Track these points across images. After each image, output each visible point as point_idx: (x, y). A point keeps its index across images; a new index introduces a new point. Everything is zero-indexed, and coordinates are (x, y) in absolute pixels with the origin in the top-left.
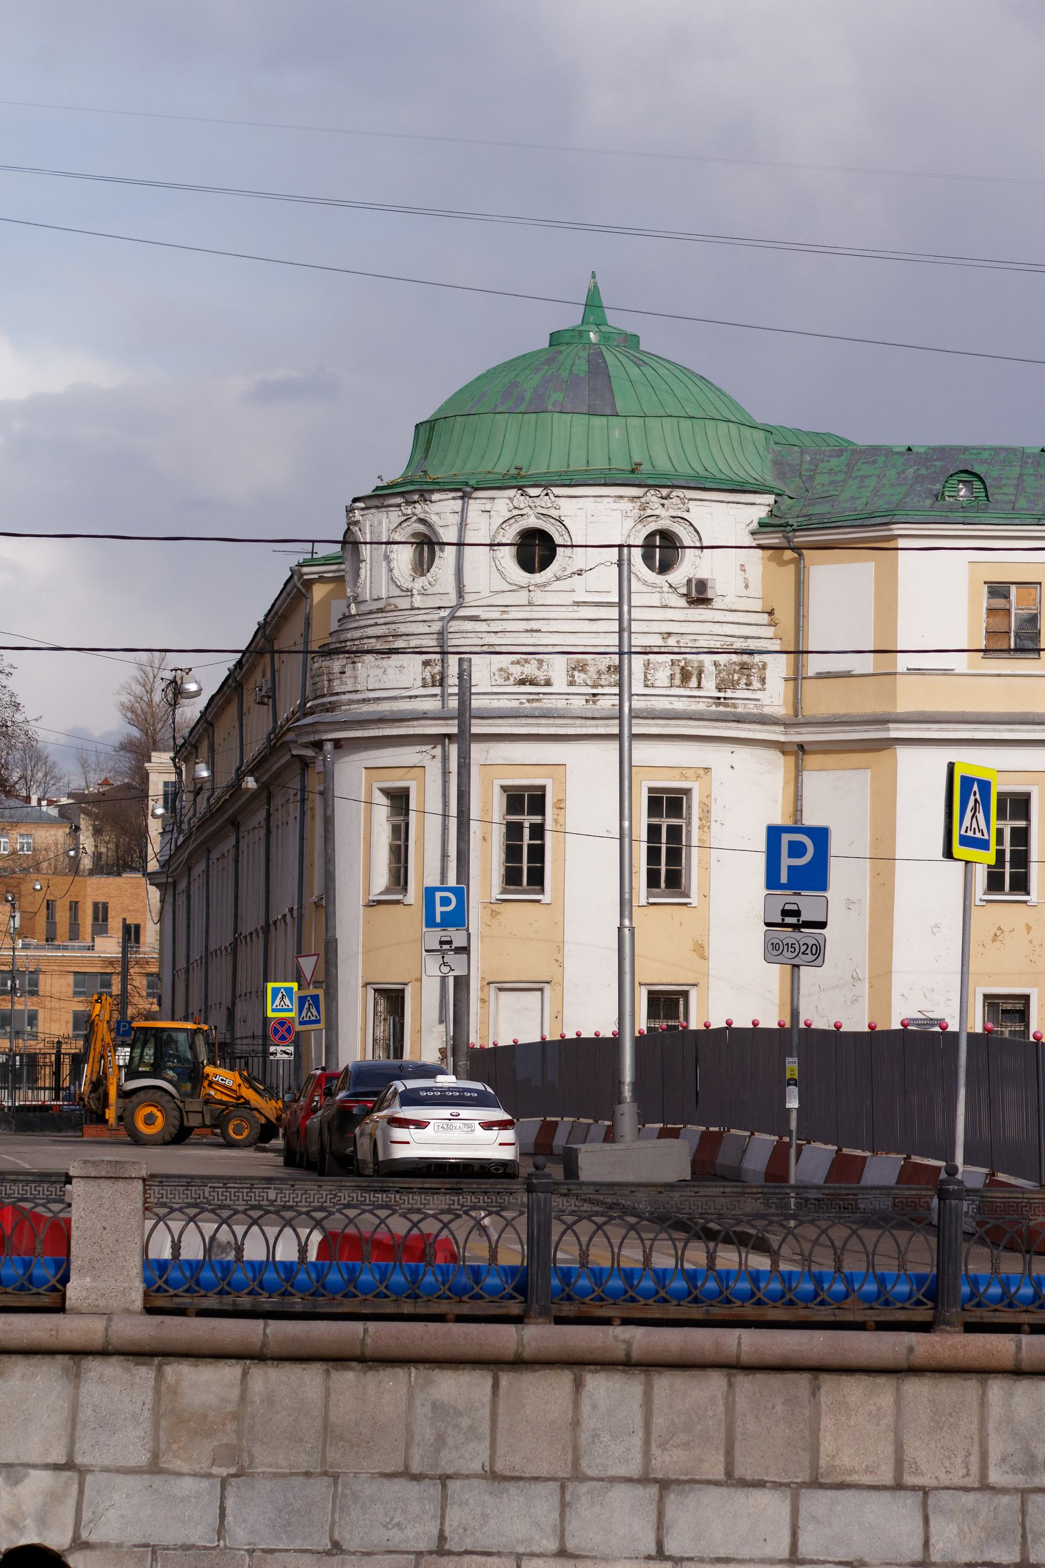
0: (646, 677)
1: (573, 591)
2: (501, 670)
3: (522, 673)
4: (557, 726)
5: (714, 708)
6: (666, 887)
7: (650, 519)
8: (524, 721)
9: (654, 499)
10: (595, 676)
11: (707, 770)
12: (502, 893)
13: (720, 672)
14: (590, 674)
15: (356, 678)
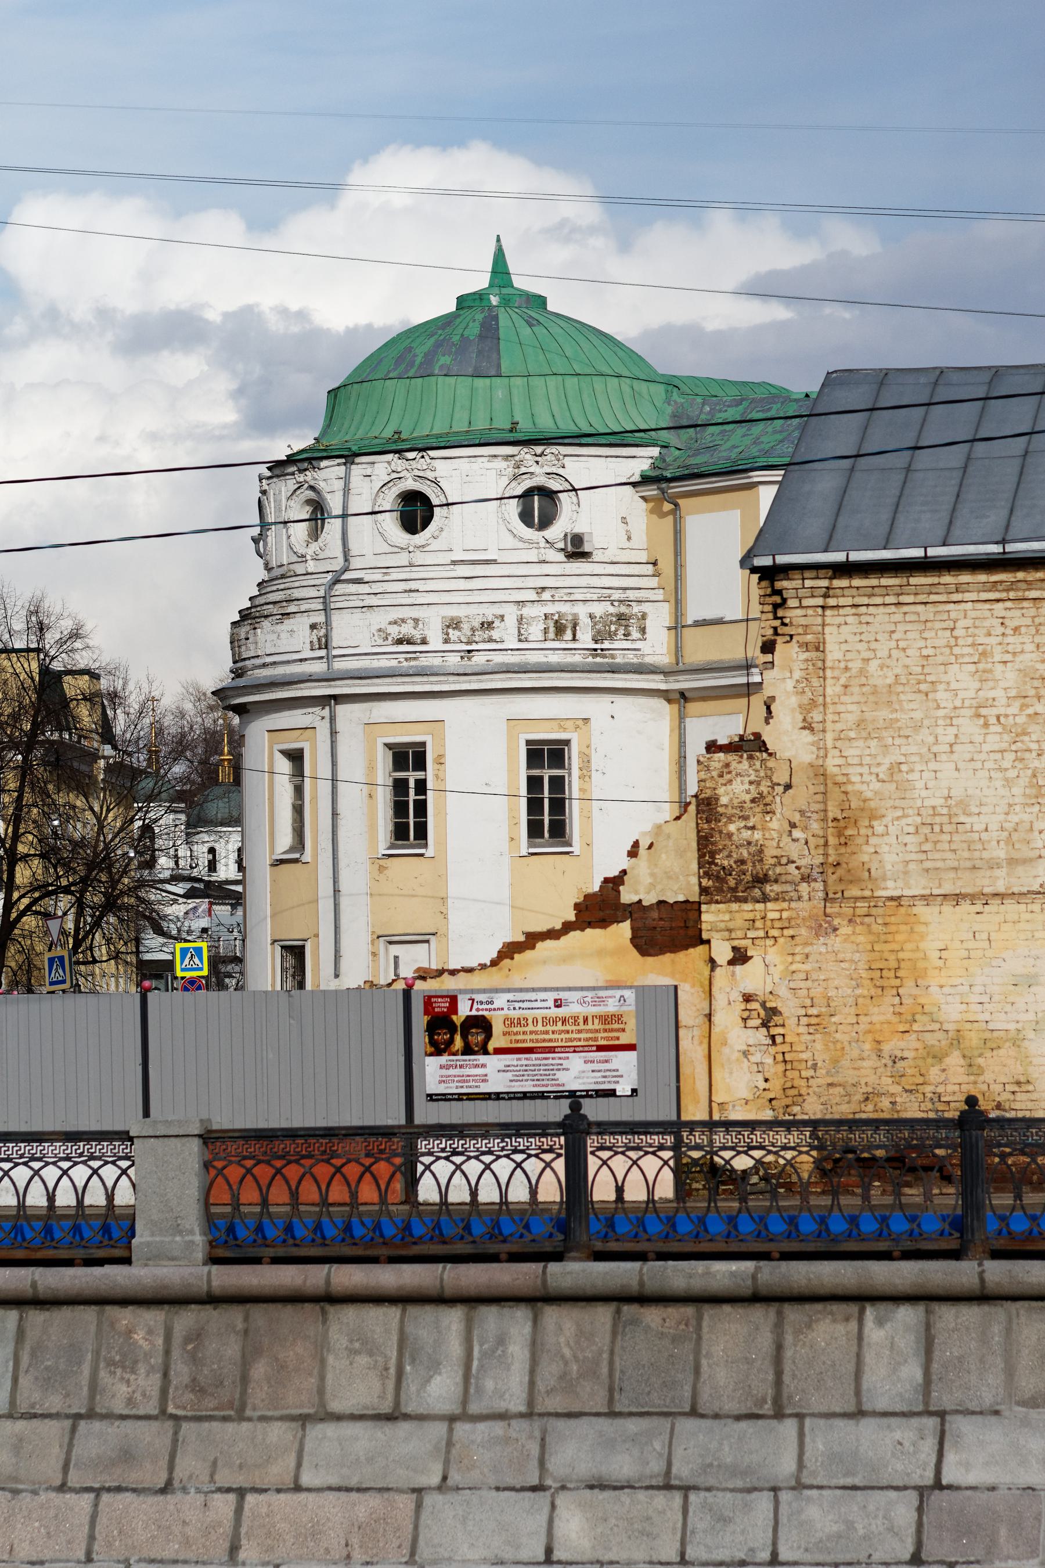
0: (519, 632)
1: (451, 550)
2: (380, 630)
3: (400, 632)
4: (432, 683)
5: (590, 659)
6: (551, 836)
7: (524, 477)
8: (400, 679)
9: (528, 456)
10: (469, 633)
11: (586, 720)
12: (389, 848)
13: (595, 624)
14: (464, 631)
15: (256, 643)
